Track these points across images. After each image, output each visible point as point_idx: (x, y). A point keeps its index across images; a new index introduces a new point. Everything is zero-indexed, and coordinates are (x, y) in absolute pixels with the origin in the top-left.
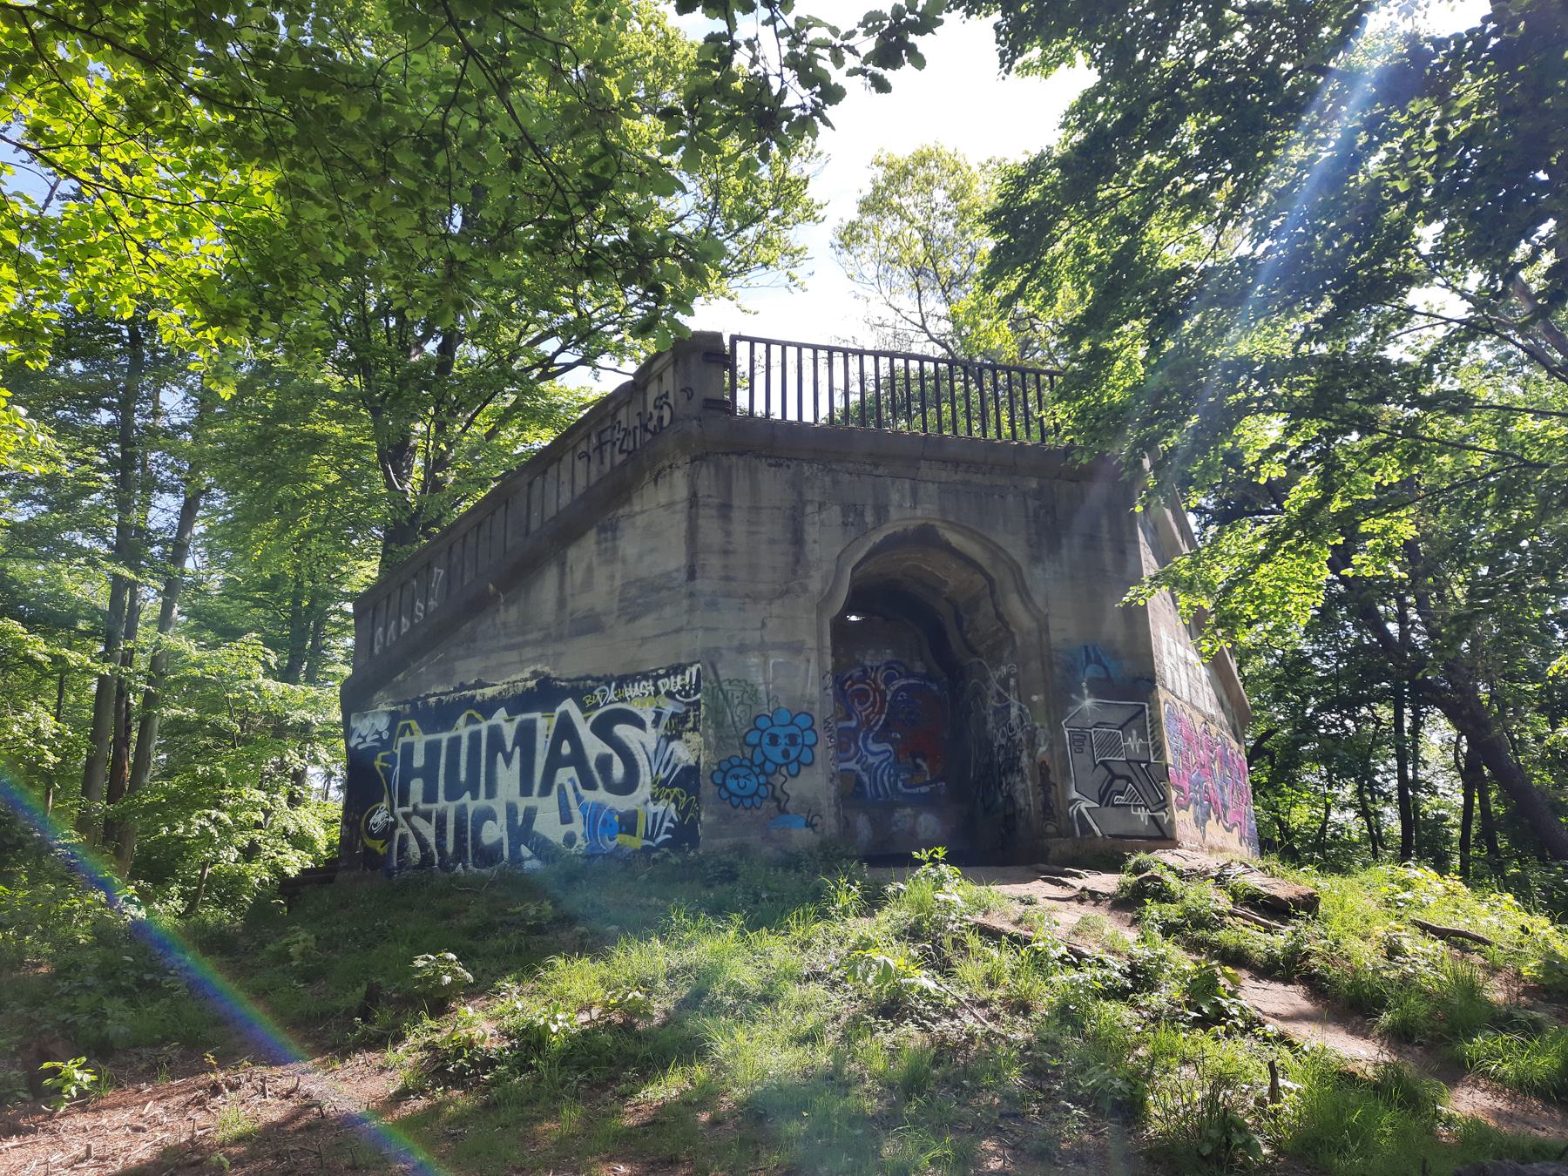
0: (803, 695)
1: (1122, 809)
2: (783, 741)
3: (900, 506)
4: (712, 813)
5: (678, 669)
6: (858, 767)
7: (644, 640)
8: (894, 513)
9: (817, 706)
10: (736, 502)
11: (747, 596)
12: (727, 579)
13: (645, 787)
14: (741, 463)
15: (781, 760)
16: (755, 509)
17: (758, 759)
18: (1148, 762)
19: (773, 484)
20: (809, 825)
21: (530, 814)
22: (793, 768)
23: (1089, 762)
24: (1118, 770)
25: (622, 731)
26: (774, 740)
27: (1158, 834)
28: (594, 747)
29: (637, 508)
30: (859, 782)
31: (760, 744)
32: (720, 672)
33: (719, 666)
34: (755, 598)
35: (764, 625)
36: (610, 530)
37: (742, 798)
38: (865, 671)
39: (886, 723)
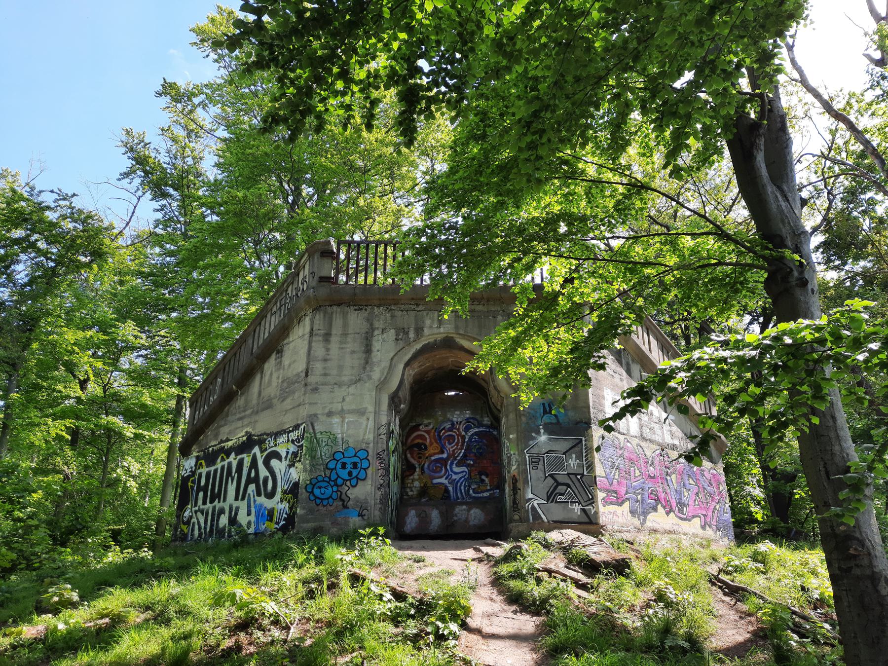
0: (363, 439)
1: (563, 505)
2: (349, 466)
3: (431, 327)
4: (304, 508)
5: (296, 427)
6: (446, 482)
7: (286, 411)
8: (426, 331)
9: (371, 445)
10: (334, 332)
11: (336, 384)
12: (325, 375)
13: (278, 495)
14: (339, 310)
15: (347, 477)
16: (345, 334)
17: (334, 477)
18: (583, 475)
19: (356, 320)
20: (360, 515)
21: (237, 509)
22: (354, 482)
23: (542, 475)
24: (560, 479)
25: (274, 463)
26: (344, 465)
27: (587, 520)
28: (263, 472)
29: (291, 339)
30: (446, 490)
31: (335, 468)
32: (316, 428)
33: (315, 424)
34: (339, 385)
35: (344, 400)
36: (280, 352)
37: (322, 500)
38: (453, 424)
39: (465, 455)
